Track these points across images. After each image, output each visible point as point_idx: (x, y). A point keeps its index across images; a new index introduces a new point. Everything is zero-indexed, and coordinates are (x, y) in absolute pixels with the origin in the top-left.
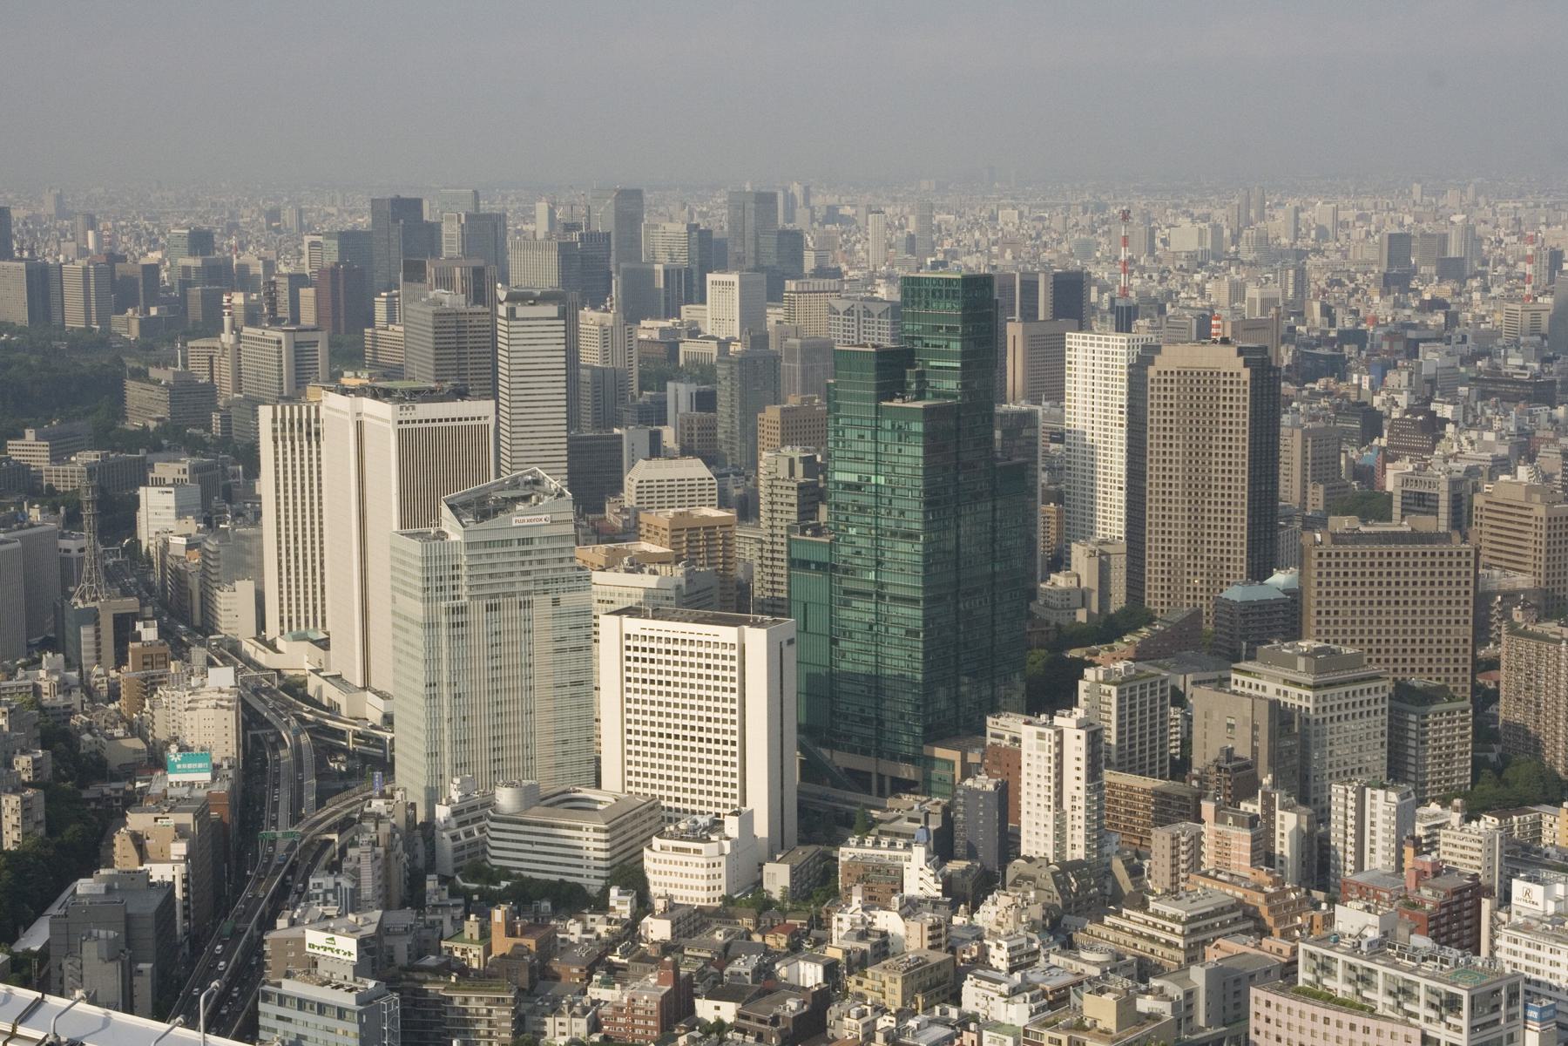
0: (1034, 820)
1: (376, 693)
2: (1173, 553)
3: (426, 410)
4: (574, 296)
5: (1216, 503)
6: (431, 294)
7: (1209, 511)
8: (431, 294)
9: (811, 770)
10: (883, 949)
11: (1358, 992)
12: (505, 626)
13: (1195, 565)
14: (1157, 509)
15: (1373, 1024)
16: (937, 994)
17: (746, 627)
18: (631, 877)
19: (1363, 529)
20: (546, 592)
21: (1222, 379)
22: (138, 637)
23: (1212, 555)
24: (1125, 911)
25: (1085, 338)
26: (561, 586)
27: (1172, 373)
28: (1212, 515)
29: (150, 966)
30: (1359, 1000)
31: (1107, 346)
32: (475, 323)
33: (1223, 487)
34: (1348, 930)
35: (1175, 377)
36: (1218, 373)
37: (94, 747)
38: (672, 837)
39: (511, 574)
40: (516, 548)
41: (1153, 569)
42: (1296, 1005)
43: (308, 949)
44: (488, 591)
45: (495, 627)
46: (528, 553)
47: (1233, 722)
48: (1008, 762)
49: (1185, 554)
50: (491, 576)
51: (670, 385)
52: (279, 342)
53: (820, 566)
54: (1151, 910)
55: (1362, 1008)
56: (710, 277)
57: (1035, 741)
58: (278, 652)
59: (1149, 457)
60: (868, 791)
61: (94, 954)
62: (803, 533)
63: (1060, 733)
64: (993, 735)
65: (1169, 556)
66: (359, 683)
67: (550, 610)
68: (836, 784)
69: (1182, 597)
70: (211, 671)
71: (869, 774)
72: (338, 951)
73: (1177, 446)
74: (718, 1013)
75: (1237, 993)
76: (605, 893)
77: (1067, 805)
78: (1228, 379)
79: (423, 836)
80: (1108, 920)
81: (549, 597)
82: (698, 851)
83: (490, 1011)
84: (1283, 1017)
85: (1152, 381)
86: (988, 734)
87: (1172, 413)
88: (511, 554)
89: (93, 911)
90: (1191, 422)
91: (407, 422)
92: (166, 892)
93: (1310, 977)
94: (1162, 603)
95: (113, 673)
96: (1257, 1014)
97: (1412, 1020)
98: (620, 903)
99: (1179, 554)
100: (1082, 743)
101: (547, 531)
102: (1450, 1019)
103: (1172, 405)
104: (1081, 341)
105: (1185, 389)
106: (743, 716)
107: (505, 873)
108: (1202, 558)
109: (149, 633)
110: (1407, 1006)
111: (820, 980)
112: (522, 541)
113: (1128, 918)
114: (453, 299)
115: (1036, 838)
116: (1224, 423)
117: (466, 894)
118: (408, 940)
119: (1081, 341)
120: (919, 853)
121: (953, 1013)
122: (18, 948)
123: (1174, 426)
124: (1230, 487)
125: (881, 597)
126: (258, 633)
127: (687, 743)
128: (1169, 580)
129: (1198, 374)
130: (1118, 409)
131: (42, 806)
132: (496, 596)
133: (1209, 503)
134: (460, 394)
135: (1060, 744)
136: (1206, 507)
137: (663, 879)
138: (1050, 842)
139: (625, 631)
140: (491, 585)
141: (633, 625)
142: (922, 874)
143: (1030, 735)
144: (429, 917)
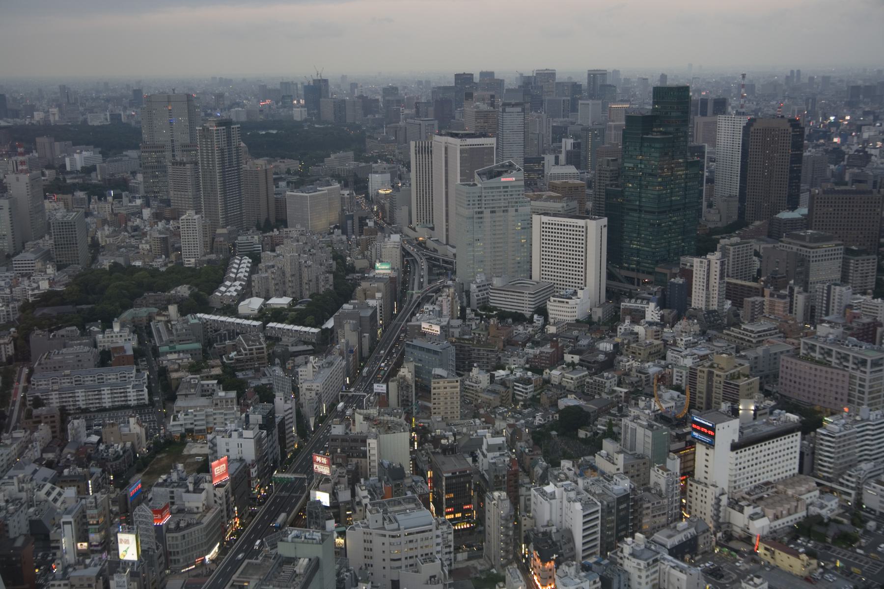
0: (697, 294)
1: (451, 246)
3: (470, 141)
4: (528, 106)
6: (475, 104)
8: (475, 104)
9: (610, 276)
11: (824, 358)
15: (829, 370)
17: (588, 220)
18: (542, 311)
19: (836, 189)
22: (367, 224)
24: (732, 328)
26: (519, 204)
30: (825, 361)
34: (822, 335)
37: (351, 262)
38: (558, 297)
39: (500, 199)
40: (502, 190)
42: (799, 362)
44: (491, 206)
46: (506, 192)
48: (688, 274)
50: (492, 200)
51: (564, 140)
55: (826, 364)
57: (699, 264)
60: (633, 284)
62: (611, 186)
63: (709, 261)
66: (445, 243)
67: (514, 213)
68: (620, 281)
70: (391, 235)
71: (634, 278)
75: (775, 359)
76: (532, 317)
77: (711, 288)
80: (725, 331)
82: (567, 303)
83: (488, 355)
88: (500, 192)
89: (349, 315)
93: (805, 352)
95: (358, 238)
96: (783, 366)
97: (846, 369)
98: (537, 320)
100: (718, 265)
101: (513, 184)
102: (862, 369)
106: (586, 250)
107: (495, 308)
110: (845, 364)
112: (504, 187)
113: (733, 331)
114: (484, 107)
115: (698, 300)
117: (481, 315)
118: (459, 330)
120: (652, 305)
121: (663, 362)
122: (324, 327)
125: (640, 211)
127: (562, 231)
134: (485, 136)
135: (709, 265)
137: (554, 312)
138: (704, 303)
140: (492, 204)
141: (545, 219)
143: (697, 262)
144: (467, 323)
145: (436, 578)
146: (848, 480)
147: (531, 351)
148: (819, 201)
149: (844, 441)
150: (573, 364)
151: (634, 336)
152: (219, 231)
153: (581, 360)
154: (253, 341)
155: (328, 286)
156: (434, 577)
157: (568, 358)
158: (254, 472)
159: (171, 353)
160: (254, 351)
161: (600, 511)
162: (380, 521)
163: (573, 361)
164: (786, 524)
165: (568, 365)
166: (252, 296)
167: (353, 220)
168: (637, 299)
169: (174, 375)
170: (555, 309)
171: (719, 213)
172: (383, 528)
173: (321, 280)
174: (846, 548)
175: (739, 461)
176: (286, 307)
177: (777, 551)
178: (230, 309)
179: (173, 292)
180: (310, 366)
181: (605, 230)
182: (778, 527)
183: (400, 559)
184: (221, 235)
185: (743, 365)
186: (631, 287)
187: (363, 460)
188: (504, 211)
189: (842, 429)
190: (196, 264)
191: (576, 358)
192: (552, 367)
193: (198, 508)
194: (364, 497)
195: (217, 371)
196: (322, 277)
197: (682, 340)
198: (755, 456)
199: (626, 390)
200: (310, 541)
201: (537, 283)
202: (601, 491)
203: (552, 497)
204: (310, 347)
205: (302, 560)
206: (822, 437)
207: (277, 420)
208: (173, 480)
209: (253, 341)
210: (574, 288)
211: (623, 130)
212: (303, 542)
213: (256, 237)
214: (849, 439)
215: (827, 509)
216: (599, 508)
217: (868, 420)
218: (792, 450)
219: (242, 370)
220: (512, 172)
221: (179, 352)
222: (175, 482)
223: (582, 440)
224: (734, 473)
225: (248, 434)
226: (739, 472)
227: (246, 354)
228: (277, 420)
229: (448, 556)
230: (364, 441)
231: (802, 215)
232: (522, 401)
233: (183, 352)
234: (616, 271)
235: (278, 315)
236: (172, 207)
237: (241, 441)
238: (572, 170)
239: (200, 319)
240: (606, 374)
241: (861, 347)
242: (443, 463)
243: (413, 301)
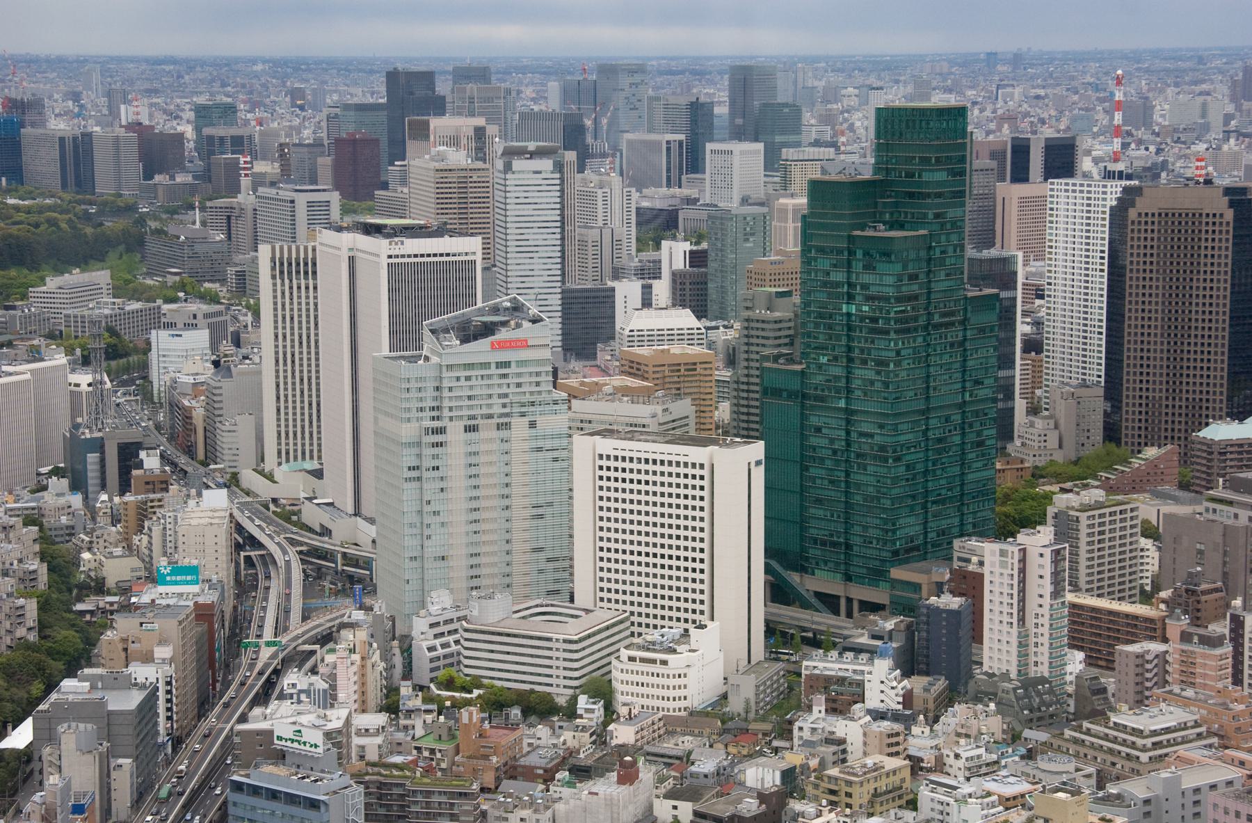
0: (996, 637)
1: (366, 519)
2: (1151, 394)
5: (1196, 344)
7: (1189, 352)
10: (842, 757)
12: (483, 447)
13: (1174, 406)
14: (1135, 350)
16: (893, 799)
18: (602, 691)
20: (523, 415)
21: (1204, 220)
22: (140, 465)
23: (1191, 396)
25: (1067, 184)
26: (538, 409)
27: (1153, 215)
28: (1192, 356)
29: (129, 761)
31: (1089, 192)
32: (475, 179)
33: (1205, 288)
35: (1156, 219)
36: (1201, 215)
40: (493, 370)
41: (1131, 386)
43: (276, 741)
44: (466, 412)
45: (473, 448)
46: (505, 376)
47: (1203, 547)
49: (1164, 395)
52: (292, 202)
53: (792, 395)
54: (1111, 724)
56: (709, 146)
57: (997, 558)
58: (275, 482)
59: (1127, 299)
60: (836, 612)
61: (73, 746)
64: (960, 559)
65: (1147, 397)
66: (350, 510)
68: (805, 605)
69: (1160, 422)
70: (205, 492)
71: (838, 597)
72: (305, 743)
73: (1156, 319)
74: (675, 812)
76: (573, 700)
77: (1031, 621)
78: (1211, 220)
79: (401, 648)
81: (526, 419)
82: (664, 663)
85: (1133, 222)
86: (955, 559)
87: (1152, 255)
90: (1172, 263)
91: (397, 256)
94: (1140, 413)
99: (1157, 395)
103: (1152, 255)
104: (1063, 187)
105: (1166, 231)
107: (476, 683)
108: (1181, 399)
111: (778, 782)
114: (459, 158)
116: (1207, 223)
119: (1063, 187)
123: (1154, 268)
124: (1213, 248)
126: (258, 465)
128: (1147, 421)
129: (1180, 215)
130: (1099, 254)
131: (35, 613)
133: (1189, 344)
135: (1023, 561)
136: (1186, 348)
139: (599, 451)
141: (607, 445)
142: (882, 687)
143: (993, 553)
151: (834, 748)
167: (103, 453)
171: (1056, 427)
181: (759, 475)
197: (957, 756)
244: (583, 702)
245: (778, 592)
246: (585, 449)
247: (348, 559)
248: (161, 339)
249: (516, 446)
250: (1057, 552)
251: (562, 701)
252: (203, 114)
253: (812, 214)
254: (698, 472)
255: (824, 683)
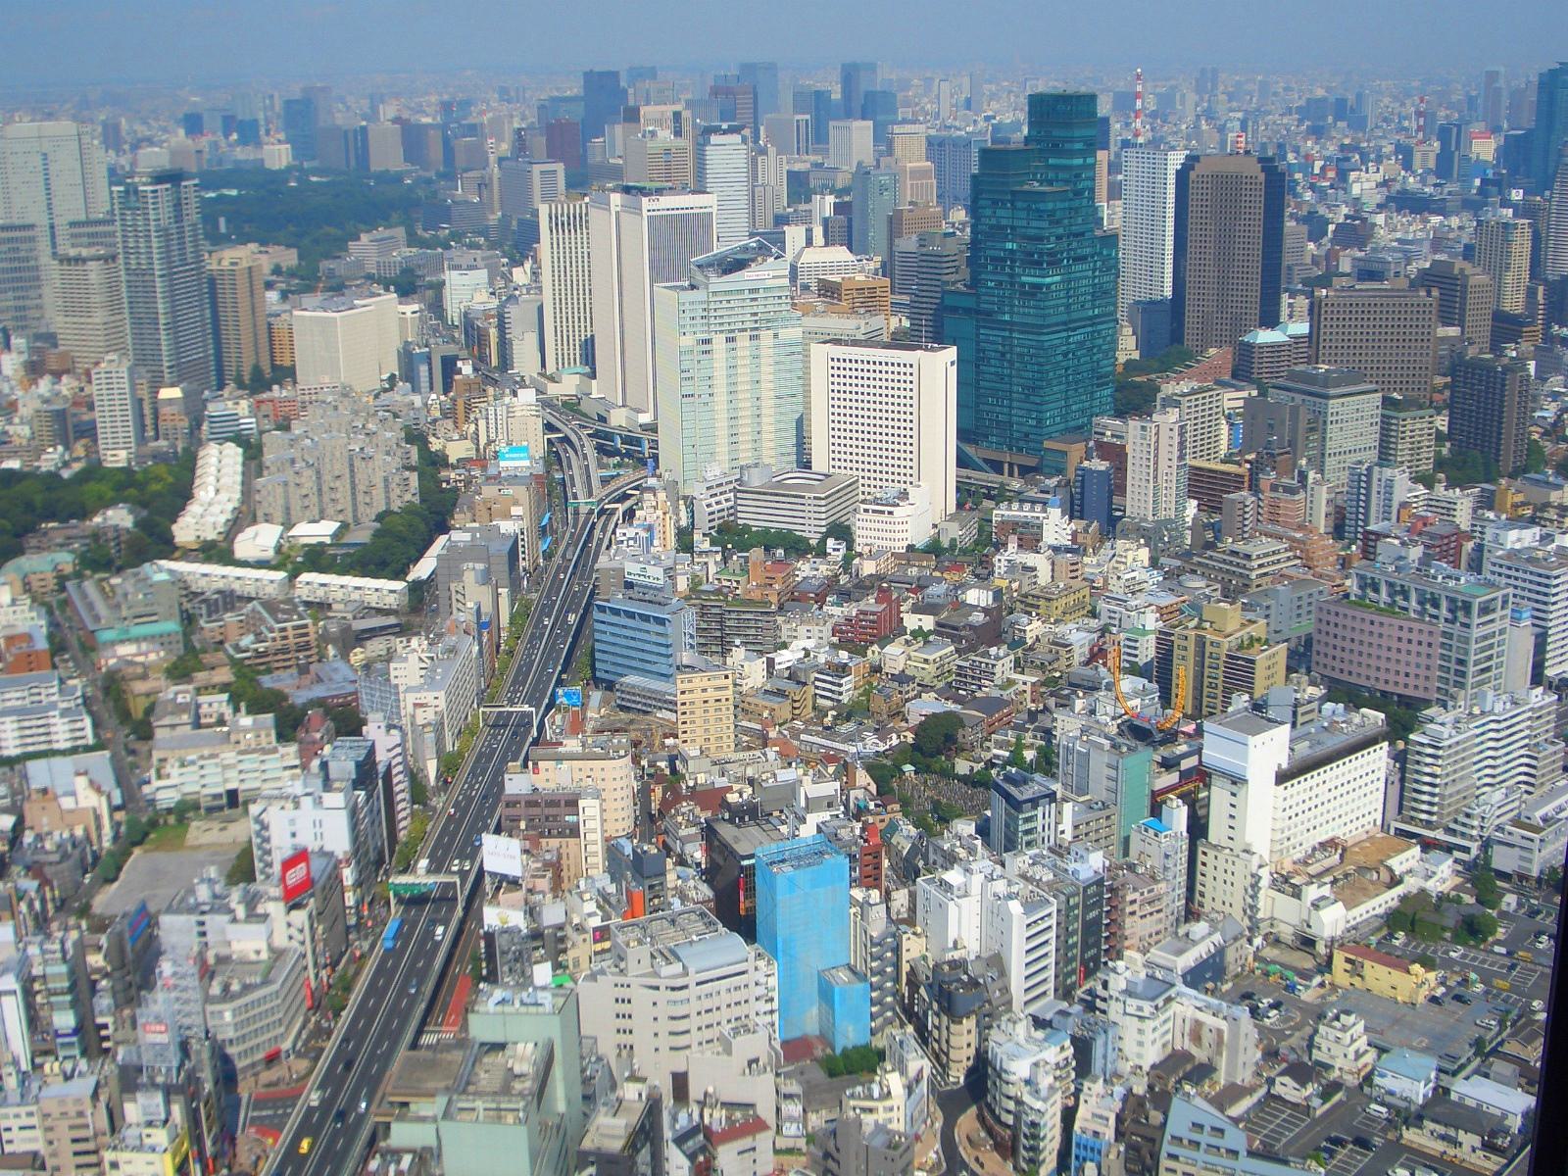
18: (842, 532)
20: (768, 329)
22: (459, 372)
46: (755, 299)
48: (1116, 455)
53: (968, 311)
76: (823, 542)
81: (771, 332)
82: (890, 513)
84: (1349, 623)
92: (510, 543)
95: (443, 398)
101: (770, 283)
109: (467, 369)
112: (751, 291)
115: (1137, 502)
120: (1055, 513)
122: (410, 578)
132: (733, 331)
143: (1135, 428)
145: (761, 1063)
146: (1464, 825)
147: (837, 611)
148: (1329, 310)
149: (1457, 753)
150: (918, 633)
152: (166, 393)
153: (938, 624)
154: (284, 612)
155: (408, 497)
156: (757, 1061)
157: (911, 621)
158: (348, 875)
159: (122, 642)
160: (290, 633)
161: (1055, 915)
162: (646, 961)
163: (920, 627)
164: (1372, 913)
165: (916, 634)
166: (254, 521)
167: (430, 364)
168: (1010, 502)
169: (140, 687)
170: (867, 530)
172: (656, 975)
173: (394, 485)
174: (1476, 947)
175: (1289, 802)
176: (328, 540)
177: (1367, 964)
178: (217, 551)
179: (98, 519)
180: (413, 658)
181: (953, 371)
182: (1359, 920)
183: (688, 1032)
184: (170, 401)
185: (1254, 622)
186: (999, 478)
187: (571, 841)
188: (751, 338)
189: (1454, 732)
190: (129, 461)
191: (928, 622)
192: (884, 641)
193: (258, 952)
194: (590, 915)
195: (224, 675)
196: (397, 479)
197: (1119, 578)
198: (1316, 791)
199: (1034, 679)
200: (533, 1009)
201: (827, 476)
202: (1051, 876)
203: (962, 893)
204: (392, 620)
205: (520, 1046)
206: (1418, 748)
207: (381, 768)
208: (200, 900)
209: (284, 612)
210: (904, 486)
211: (974, 176)
212: (518, 1013)
213: (244, 404)
214: (1464, 750)
215: (1436, 878)
216: (1054, 909)
217: (1491, 712)
218: (1372, 777)
219: (269, 671)
220: (764, 260)
221: (137, 640)
222: (204, 904)
223: (964, 779)
224: (1279, 825)
225: (336, 799)
226: (1288, 822)
227: (274, 639)
228: (381, 768)
229: (768, 1018)
230: (572, 803)
231: (1290, 336)
232: (832, 709)
233: (145, 639)
234: (970, 450)
235: (317, 558)
236: (61, 348)
237: (319, 814)
238: (840, 254)
239: (171, 572)
240: (993, 650)
241: (1458, 579)
242: (737, 839)
243: (582, 519)
244: (831, 543)
245: (963, 461)
246: (820, 353)
247: (627, 440)
248: (452, 278)
249: (764, 352)
250: (1182, 427)
251: (813, 542)
252: (446, 107)
253: (982, 174)
254: (909, 370)
255: (1013, 526)
